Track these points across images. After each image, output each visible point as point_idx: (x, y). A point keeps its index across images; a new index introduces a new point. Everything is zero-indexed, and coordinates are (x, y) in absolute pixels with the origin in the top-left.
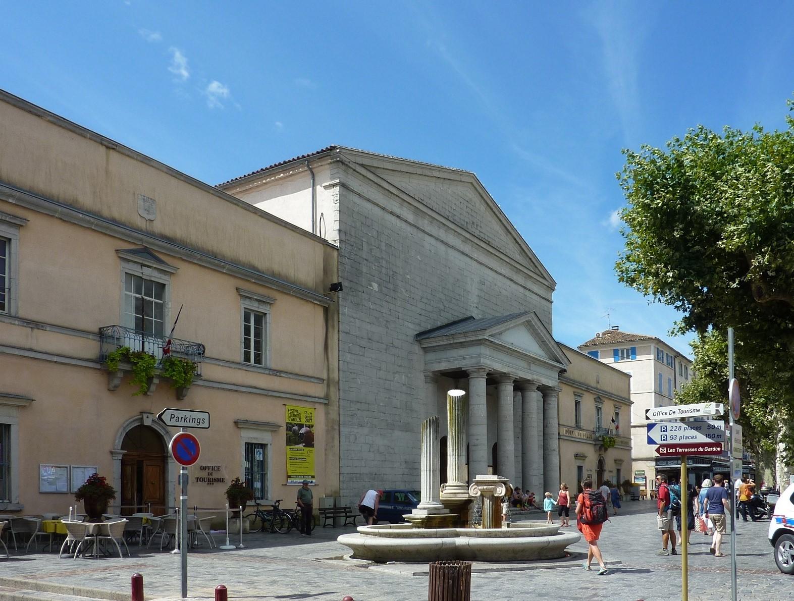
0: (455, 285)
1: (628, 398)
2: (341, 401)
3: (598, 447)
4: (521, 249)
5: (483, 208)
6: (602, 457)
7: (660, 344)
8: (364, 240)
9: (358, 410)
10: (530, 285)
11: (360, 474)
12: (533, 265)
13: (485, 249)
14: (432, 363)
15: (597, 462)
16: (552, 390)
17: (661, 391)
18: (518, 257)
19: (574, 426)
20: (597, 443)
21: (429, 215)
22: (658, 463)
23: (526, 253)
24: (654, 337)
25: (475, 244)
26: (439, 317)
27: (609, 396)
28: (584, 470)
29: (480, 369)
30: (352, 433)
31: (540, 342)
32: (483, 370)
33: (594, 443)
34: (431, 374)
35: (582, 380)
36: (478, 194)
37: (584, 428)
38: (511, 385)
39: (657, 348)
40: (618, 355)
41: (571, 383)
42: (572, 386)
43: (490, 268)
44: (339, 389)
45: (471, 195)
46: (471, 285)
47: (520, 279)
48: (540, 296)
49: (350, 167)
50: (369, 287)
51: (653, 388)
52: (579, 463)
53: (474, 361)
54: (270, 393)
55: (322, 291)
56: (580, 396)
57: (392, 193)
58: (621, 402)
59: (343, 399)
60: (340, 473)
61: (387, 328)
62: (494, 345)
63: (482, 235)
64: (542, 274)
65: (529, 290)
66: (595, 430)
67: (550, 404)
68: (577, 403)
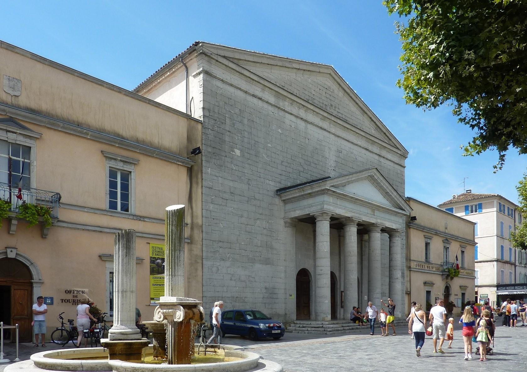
1: (472, 239)
3: (444, 277)
4: (376, 126)
5: (341, 94)
6: (449, 284)
7: (502, 200)
9: (221, 247)
10: (384, 153)
18: (373, 132)
20: (444, 273)
21: (289, 98)
22: (499, 288)
23: (381, 129)
24: (496, 195)
29: (323, 213)
30: (214, 266)
32: (326, 214)
33: (441, 273)
35: (432, 227)
37: (433, 262)
39: (508, 207)
40: (468, 210)
43: (346, 140)
44: (202, 232)
45: (329, 83)
47: (375, 149)
48: (394, 162)
49: (212, 58)
53: (319, 207)
58: (466, 243)
61: (249, 184)
63: (340, 115)
64: (396, 146)
66: (442, 264)
67: (394, 243)
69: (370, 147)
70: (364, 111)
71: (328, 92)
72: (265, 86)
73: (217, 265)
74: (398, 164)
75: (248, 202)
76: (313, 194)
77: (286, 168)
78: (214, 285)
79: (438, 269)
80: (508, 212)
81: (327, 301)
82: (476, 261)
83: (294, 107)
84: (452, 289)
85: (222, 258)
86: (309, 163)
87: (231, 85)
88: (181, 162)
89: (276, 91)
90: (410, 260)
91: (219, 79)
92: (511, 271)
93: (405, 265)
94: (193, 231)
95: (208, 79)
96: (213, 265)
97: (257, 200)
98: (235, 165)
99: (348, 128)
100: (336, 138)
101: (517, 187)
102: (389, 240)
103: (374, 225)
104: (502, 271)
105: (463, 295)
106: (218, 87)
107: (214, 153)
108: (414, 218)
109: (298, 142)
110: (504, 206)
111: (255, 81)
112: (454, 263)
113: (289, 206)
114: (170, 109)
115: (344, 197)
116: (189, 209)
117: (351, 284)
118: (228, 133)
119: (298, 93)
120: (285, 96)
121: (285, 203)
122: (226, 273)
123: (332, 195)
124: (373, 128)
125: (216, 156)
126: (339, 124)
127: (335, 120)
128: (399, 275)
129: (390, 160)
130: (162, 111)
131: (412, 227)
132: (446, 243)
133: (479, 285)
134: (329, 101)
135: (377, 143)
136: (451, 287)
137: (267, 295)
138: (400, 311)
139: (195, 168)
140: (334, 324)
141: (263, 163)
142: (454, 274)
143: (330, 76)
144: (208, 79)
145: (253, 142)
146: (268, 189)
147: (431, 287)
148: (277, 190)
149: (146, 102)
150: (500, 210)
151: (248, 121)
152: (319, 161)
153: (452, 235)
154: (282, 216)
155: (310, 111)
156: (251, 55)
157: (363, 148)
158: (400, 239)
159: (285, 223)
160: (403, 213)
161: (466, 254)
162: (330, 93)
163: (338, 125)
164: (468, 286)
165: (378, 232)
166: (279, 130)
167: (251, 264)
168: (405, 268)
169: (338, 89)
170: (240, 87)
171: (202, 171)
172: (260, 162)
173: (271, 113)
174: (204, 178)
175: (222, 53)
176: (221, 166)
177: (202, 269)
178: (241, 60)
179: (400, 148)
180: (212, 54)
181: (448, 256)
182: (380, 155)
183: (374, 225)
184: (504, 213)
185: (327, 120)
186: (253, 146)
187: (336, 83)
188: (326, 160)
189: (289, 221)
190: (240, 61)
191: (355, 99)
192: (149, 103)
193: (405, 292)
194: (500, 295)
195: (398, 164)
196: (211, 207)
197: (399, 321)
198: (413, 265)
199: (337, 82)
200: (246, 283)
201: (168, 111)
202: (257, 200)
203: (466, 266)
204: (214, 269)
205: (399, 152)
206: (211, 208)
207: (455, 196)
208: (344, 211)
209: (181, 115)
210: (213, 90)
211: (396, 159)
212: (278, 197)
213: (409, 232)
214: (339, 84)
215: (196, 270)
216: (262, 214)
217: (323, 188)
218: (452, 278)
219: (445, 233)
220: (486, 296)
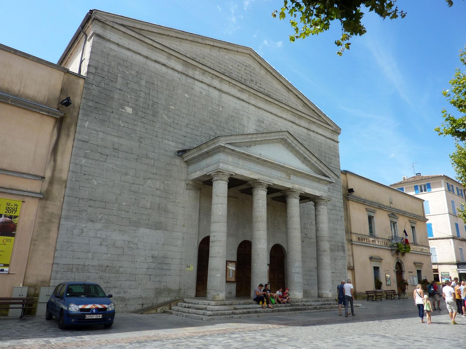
0: (228, 119)
1: (422, 215)
2: (65, 197)
3: (394, 252)
4: (303, 103)
5: (263, 72)
6: (400, 260)
7: (449, 180)
8: (119, 75)
9: (90, 207)
10: (313, 127)
11: (84, 265)
12: (316, 114)
13: (263, 98)
15: (395, 264)
16: (320, 199)
17: (455, 213)
18: (300, 108)
19: (368, 235)
20: (393, 248)
21: (200, 68)
22: (460, 266)
23: (308, 106)
24: (442, 175)
25: (252, 94)
27: (403, 213)
28: (381, 271)
29: (219, 172)
30: (77, 227)
31: (303, 159)
32: (222, 173)
33: (390, 248)
34: (191, 182)
35: (375, 200)
36: (257, 62)
37: (379, 236)
39: (457, 187)
40: (418, 189)
41: (361, 201)
42: (364, 204)
43: (269, 112)
44: (66, 187)
45: (249, 62)
46: (248, 122)
47: (303, 123)
48: (325, 137)
49: (107, 24)
50: (120, 109)
51: (448, 211)
53: (215, 166)
55: (56, 106)
56: (373, 212)
57: (156, 48)
58: (416, 219)
59: (68, 196)
61: (141, 142)
62: (236, 153)
63: (261, 89)
64: (326, 122)
65: (313, 131)
66: (390, 238)
67: (320, 211)
69: (297, 121)
70: (289, 89)
71: (248, 69)
72: (171, 54)
73: (82, 227)
74: (330, 139)
75: (137, 159)
76: (210, 153)
77: (192, 131)
78: (73, 250)
79: (386, 244)
80: (458, 192)
81: (219, 275)
82: (429, 238)
83: (206, 76)
84: (405, 265)
85: (90, 219)
86: (222, 128)
87: (129, 49)
88: (45, 111)
89: (184, 60)
90: (351, 233)
91: (114, 43)
92: (461, 247)
93: (345, 238)
94: (52, 186)
95: (99, 41)
96: (76, 226)
97: (150, 158)
98: (123, 122)
99: (270, 102)
100: (257, 109)
101: (451, 156)
102: (314, 209)
103: (290, 190)
104: (461, 249)
105: (419, 272)
106: (111, 49)
107: (96, 108)
108: (351, 191)
109: (209, 108)
110: (452, 186)
111: (159, 49)
112: (403, 238)
113: (192, 168)
114: (42, 61)
115: (249, 158)
116: (50, 161)
117: (258, 255)
118: (118, 91)
119: (212, 66)
120: (195, 66)
121: (188, 165)
122: (95, 236)
123: (232, 154)
124: (301, 105)
125: (98, 111)
126: (260, 97)
127: (255, 93)
128: (326, 247)
129: (321, 135)
130: (32, 62)
131: (350, 199)
132: (393, 217)
133: (439, 262)
134: (249, 76)
135: (304, 117)
136: (403, 263)
137: (154, 265)
138: (330, 289)
139: (68, 120)
140: (225, 305)
141: (162, 123)
142: (404, 249)
143: (250, 56)
144: (99, 41)
145: (151, 102)
146: (167, 149)
147: (379, 263)
148: (178, 151)
149: (11, 52)
150: (449, 190)
151: (146, 83)
152: (235, 128)
153: (398, 210)
154: (184, 176)
155: (225, 82)
156: (155, 27)
157: (289, 121)
158: (325, 207)
159: (187, 185)
160: (327, 179)
161: (416, 229)
162: (251, 70)
163: (260, 98)
164: (423, 263)
165: (296, 198)
166: (186, 95)
167: (133, 228)
168: (345, 241)
169: (260, 68)
170: (139, 52)
171: (77, 124)
172: (158, 121)
173: (177, 79)
174: (77, 130)
175: (120, 22)
176: (105, 121)
177: (58, 230)
178: (143, 30)
179: (331, 125)
180: (106, 21)
181: (397, 230)
182: (308, 129)
183: (290, 190)
184: (453, 192)
185: (246, 92)
186: (150, 106)
187: (256, 62)
188: (244, 128)
189: (191, 183)
190: (143, 31)
191: (278, 77)
192: (14, 53)
193: (346, 267)
194: (462, 273)
195: (330, 139)
196: (83, 161)
197: (325, 303)
198: (354, 238)
199: (258, 62)
200: (123, 250)
201: (39, 63)
202: (150, 158)
203: (418, 241)
204: (76, 231)
205: (330, 128)
206: (83, 162)
207: (404, 177)
208: (248, 172)
209: (56, 68)
210: (105, 50)
211: (328, 134)
212: (179, 158)
213: (348, 204)
214: (260, 64)
215: (49, 231)
216: (155, 174)
217: (217, 145)
218: (403, 254)
219: (390, 207)
220: (447, 274)
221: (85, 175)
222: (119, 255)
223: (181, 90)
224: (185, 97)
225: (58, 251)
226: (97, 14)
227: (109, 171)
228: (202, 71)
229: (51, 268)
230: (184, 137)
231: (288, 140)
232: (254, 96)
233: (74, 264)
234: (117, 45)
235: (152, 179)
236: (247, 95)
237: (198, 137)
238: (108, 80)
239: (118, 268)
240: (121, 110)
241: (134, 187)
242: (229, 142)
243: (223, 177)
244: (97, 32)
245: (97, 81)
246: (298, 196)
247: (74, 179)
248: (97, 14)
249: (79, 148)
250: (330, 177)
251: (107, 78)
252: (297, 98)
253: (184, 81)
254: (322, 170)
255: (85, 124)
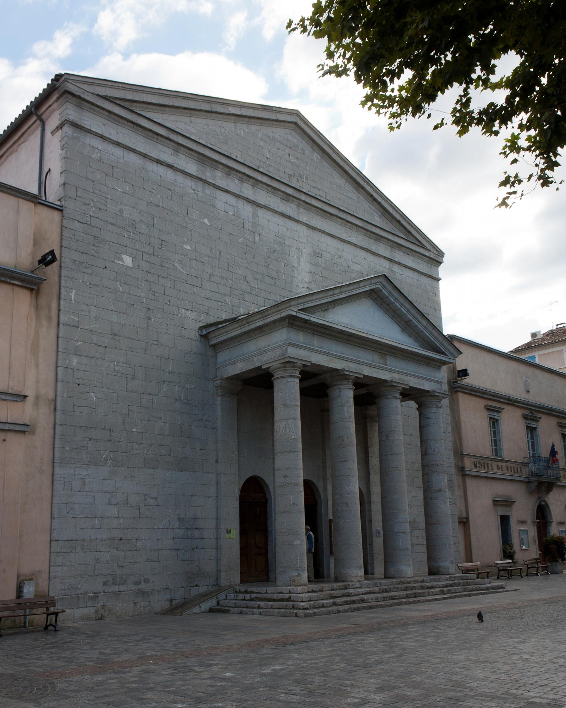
0: (269, 257)
3: (533, 486)
4: (382, 210)
9: (91, 439)
10: (399, 256)
11: (91, 540)
14: (225, 366)
15: (535, 508)
18: (377, 220)
21: (223, 165)
25: (302, 203)
26: (243, 302)
30: (76, 477)
32: (292, 365)
38: (349, 388)
46: (298, 258)
47: (383, 250)
50: (116, 261)
52: (503, 511)
53: (278, 352)
54: (377, 524)
60: (51, 540)
67: (429, 418)
68: (494, 422)
95: (75, 135)
96: (75, 475)
100: (311, 231)
106: (93, 147)
119: (239, 156)
124: (377, 213)
141: (175, 279)
163: (314, 209)
166: (206, 221)
179: (429, 247)
196: (75, 361)
198: (468, 463)
206: (74, 364)
221: (79, 385)
222: (134, 518)
223: (198, 212)
224: (204, 223)
225: (55, 518)
226: (69, 81)
227: (110, 376)
228: (227, 170)
229: (49, 548)
230: (207, 300)
231: (383, 290)
232: (307, 205)
233: (78, 539)
234: (101, 138)
235: (168, 383)
236: (294, 207)
237: (227, 297)
238: (94, 209)
239: (135, 541)
240: (118, 262)
241: (145, 400)
242: (302, 307)
243: (294, 371)
244: (71, 118)
245: (79, 213)
246: (399, 394)
247: (65, 395)
248: (69, 81)
249: (66, 340)
250: (446, 353)
251: (92, 204)
252: (372, 200)
253: (200, 194)
254: (435, 342)
255: (71, 294)
